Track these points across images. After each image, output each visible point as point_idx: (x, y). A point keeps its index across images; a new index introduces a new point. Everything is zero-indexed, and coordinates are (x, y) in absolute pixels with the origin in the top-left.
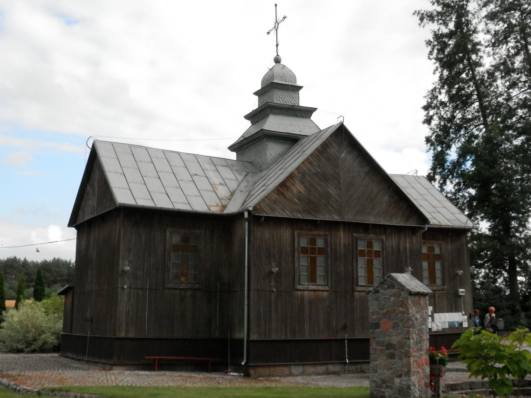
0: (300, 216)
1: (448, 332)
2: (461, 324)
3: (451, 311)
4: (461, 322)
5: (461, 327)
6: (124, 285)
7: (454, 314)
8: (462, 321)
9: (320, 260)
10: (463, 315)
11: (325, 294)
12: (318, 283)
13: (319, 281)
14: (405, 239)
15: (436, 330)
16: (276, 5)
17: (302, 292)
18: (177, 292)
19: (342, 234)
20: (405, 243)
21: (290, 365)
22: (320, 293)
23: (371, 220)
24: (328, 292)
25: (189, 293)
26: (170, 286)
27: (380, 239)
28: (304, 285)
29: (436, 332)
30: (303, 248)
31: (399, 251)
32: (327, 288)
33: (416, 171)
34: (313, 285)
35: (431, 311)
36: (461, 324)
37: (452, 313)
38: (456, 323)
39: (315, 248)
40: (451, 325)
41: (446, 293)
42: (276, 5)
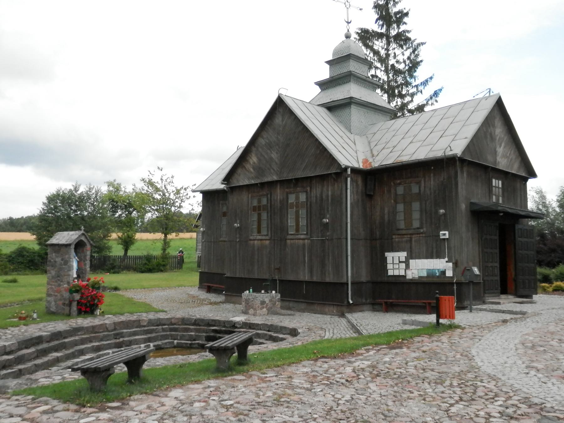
0: (253, 182)
1: (425, 280)
2: (444, 272)
3: (432, 258)
4: (443, 270)
5: (442, 276)
7: (435, 260)
9: (264, 216)
10: (447, 262)
11: (268, 242)
12: (262, 234)
13: (264, 232)
14: (328, 186)
15: (411, 278)
19: (278, 191)
20: (328, 191)
22: (264, 241)
23: (300, 174)
29: (411, 280)
31: (322, 199)
32: (267, 238)
36: (444, 272)
37: (432, 260)
39: (261, 206)
40: (431, 274)
41: (425, 237)
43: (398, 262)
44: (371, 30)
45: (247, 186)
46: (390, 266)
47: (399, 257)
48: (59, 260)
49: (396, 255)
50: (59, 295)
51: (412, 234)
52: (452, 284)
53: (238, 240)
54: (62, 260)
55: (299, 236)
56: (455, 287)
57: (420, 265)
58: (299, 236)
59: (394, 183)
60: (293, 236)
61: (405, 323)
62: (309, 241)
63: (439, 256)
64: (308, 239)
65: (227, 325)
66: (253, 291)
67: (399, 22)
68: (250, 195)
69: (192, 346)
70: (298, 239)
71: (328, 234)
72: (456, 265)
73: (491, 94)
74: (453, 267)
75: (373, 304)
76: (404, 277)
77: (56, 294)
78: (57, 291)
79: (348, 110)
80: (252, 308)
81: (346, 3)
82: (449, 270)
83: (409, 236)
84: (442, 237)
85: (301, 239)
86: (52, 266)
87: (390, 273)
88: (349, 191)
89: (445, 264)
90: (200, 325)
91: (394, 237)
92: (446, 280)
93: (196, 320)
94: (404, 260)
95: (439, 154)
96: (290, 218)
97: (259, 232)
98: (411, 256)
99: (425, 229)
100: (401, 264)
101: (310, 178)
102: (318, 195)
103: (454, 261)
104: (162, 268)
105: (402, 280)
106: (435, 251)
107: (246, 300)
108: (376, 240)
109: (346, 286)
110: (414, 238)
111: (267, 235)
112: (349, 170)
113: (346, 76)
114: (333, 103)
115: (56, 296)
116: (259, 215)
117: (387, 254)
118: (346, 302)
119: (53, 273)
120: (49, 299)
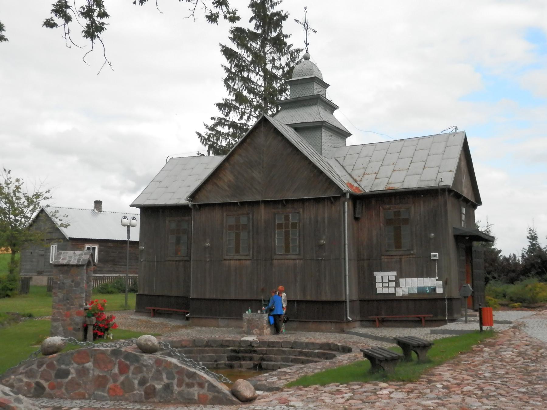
1: (416, 297)
2: (434, 289)
6: (142, 259)
8: (435, 286)
9: (243, 235)
10: (437, 280)
11: (248, 262)
15: (401, 295)
16: (305, 9)
17: (230, 261)
18: (174, 263)
21: (218, 318)
22: (244, 261)
24: (250, 261)
25: (181, 264)
26: (168, 259)
27: (297, 212)
28: (230, 256)
30: (230, 226)
31: (317, 222)
33: (455, 127)
34: (238, 255)
35: (395, 276)
36: (434, 289)
37: (422, 279)
38: (427, 289)
40: (421, 290)
41: (415, 258)
42: (305, 9)
43: (387, 281)
44: (247, 29)
45: (220, 204)
46: (378, 285)
47: (389, 276)
48: (68, 282)
49: (386, 274)
50: (68, 319)
51: (402, 255)
52: (444, 299)
53: (208, 260)
54: (73, 282)
55: (289, 257)
56: (446, 302)
57: (410, 283)
58: (289, 257)
59: (383, 208)
60: (281, 256)
61: (433, 332)
62: (302, 261)
63: (429, 275)
64: (300, 259)
65: (243, 346)
66: (252, 312)
67: (277, 25)
68: (225, 214)
69: (219, 366)
70: (287, 259)
71: (324, 254)
72: (445, 284)
73: (457, 131)
74: (443, 285)
75: (361, 321)
76: (394, 294)
77: (65, 318)
78: (66, 316)
79: (318, 133)
80: (257, 327)
81: (305, 24)
82: (439, 287)
83: (398, 257)
84: (432, 258)
85: (291, 259)
86: (59, 288)
87: (379, 291)
88: (346, 214)
89: (435, 282)
90: (212, 347)
91: (383, 257)
92: (438, 297)
93: (208, 342)
94: (394, 279)
95: (432, 184)
96: (278, 238)
97: (237, 251)
98: (401, 275)
99: (415, 251)
100: (390, 283)
101: (303, 201)
102: (312, 217)
103: (445, 279)
104: (9, 292)
105: (391, 298)
106: (425, 270)
107: (248, 320)
108: (363, 260)
109: (345, 304)
110: (404, 259)
111: (248, 255)
112: (348, 195)
113: (315, 98)
114: (302, 124)
115: (63, 320)
116: (238, 236)
117: (375, 274)
118: (345, 319)
119: (61, 296)
120: (55, 324)
